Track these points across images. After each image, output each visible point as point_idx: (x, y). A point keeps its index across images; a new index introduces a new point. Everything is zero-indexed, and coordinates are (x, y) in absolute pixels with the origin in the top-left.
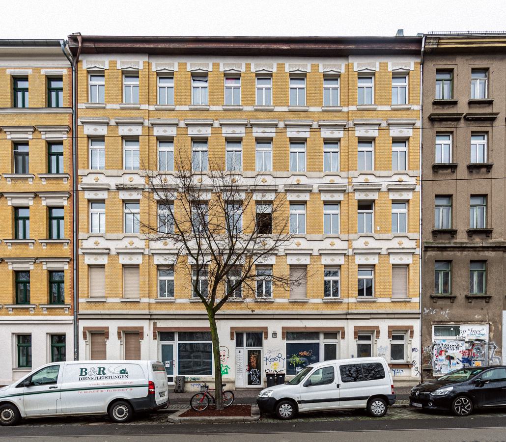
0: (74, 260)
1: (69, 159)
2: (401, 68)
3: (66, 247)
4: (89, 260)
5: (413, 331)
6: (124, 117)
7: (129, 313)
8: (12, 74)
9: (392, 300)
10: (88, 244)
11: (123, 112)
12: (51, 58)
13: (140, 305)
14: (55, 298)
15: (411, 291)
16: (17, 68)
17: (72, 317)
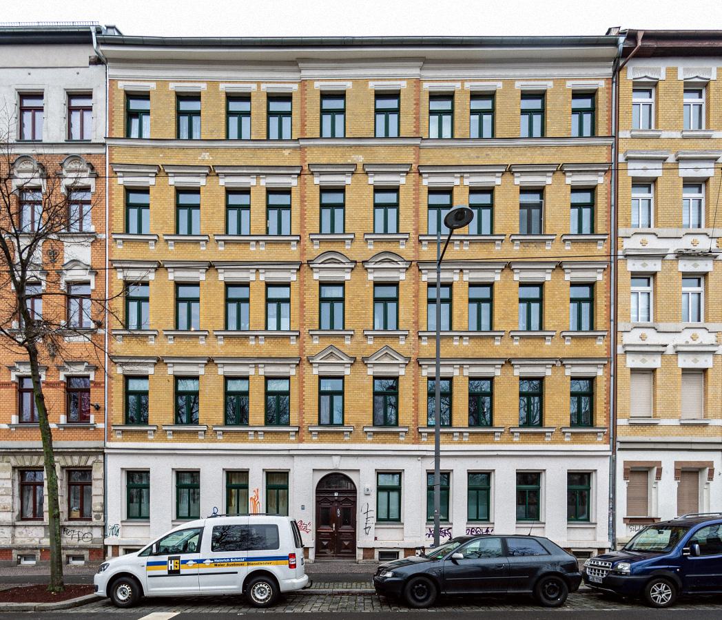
0: (611, 361)
1: (606, 212)
2: (697, 77)
3: (600, 343)
4: (633, 362)
5: (713, 470)
6: (689, 149)
7: (693, 441)
8: (126, 89)
9: (682, 422)
10: (630, 338)
11: (687, 143)
12: (561, 64)
13: (659, 429)
14: (583, 419)
15: (710, 411)
16: (530, 80)
17: (608, 447)
